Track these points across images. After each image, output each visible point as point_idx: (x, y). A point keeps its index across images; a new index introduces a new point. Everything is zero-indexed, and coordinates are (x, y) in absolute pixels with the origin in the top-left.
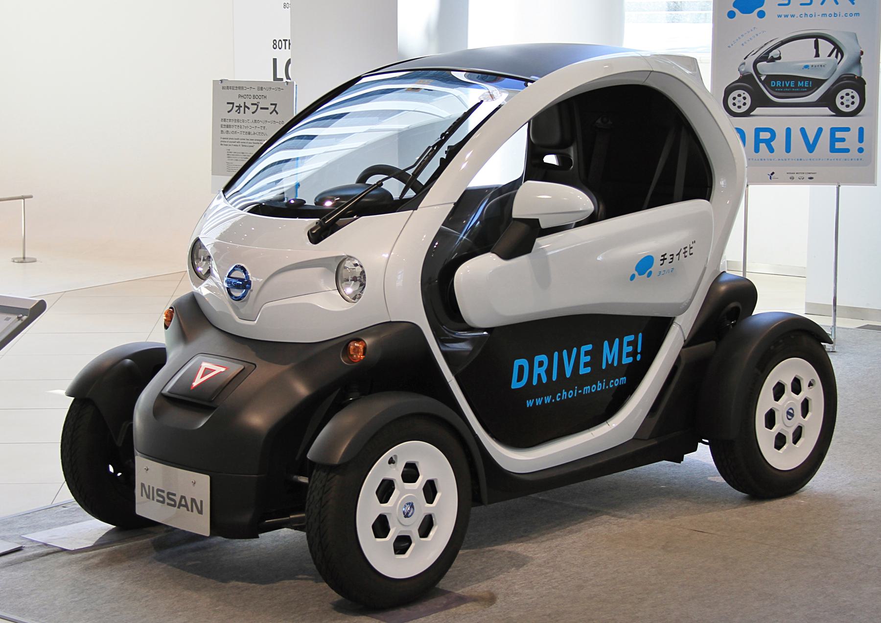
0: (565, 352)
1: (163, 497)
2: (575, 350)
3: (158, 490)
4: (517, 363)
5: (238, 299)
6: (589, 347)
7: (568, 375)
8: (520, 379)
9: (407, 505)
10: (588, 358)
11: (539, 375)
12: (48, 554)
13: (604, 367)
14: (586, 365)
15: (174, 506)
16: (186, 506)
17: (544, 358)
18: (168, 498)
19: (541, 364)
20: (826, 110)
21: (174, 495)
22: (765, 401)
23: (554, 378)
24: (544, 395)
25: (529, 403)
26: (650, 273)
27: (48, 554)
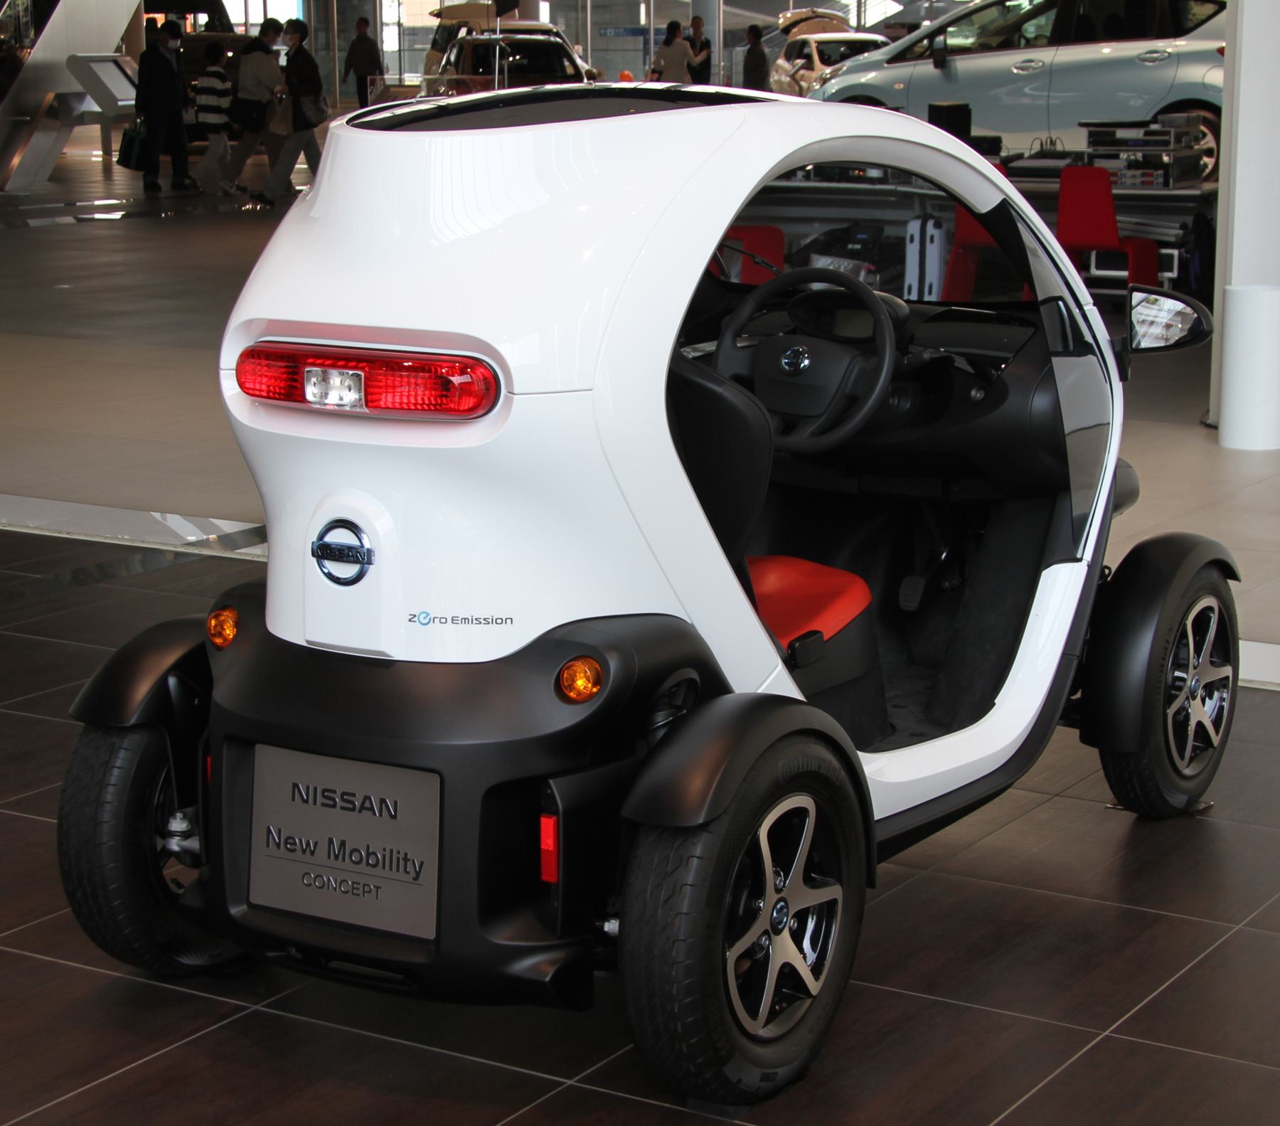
1: (353, 803)
3: (324, 791)
15: (353, 809)
16: (372, 809)
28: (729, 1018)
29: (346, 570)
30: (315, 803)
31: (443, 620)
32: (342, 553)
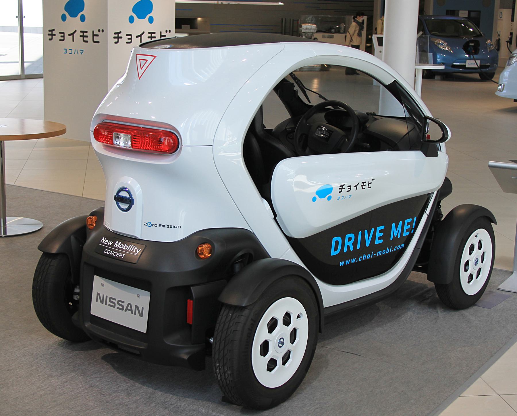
0: (366, 231)
1: (123, 306)
2: (373, 230)
3: (110, 298)
4: (334, 239)
5: (282, 338)
6: (382, 227)
7: (367, 245)
8: (336, 249)
9: (280, 341)
10: (381, 234)
11: (348, 246)
13: (391, 239)
14: (380, 238)
15: (122, 309)
16: (131, 310)
17: (352, 235)
18: (112, 302)
19: (350, 239)
21: (123, 302)
22: (261, 334)
23: (358, 248)
24: (351, 258)
25: (342, 264)
28: (504, 292)
29: (125, 206)
30: (106, 304)
31: (156, 225)
32: (125, 200)
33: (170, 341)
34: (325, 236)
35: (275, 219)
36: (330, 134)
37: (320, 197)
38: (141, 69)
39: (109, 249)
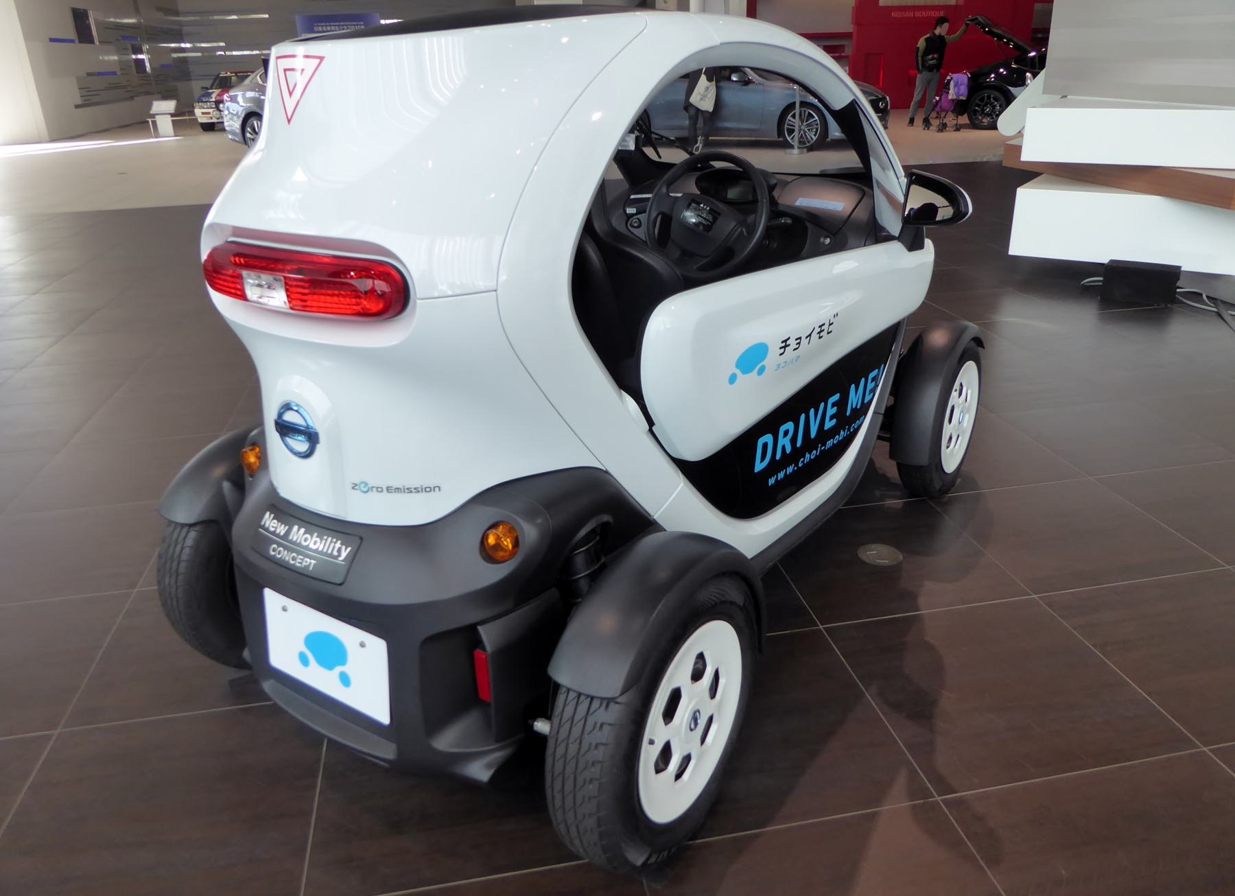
0: (812, 412)
4: (761, 442)
6: (836, 397)
8: (763, 459)
11: (784, 447)
12: (579, 749)
20: (904, 181)
25: (772, 481)
26: (763, 368)
27: (579, 749)
33: (446, 741)
34: (744, 444)
35: (651, 431)
36: (715, 219)
37: (744, 372)
38: (291, 94)
39: (280, 545)
